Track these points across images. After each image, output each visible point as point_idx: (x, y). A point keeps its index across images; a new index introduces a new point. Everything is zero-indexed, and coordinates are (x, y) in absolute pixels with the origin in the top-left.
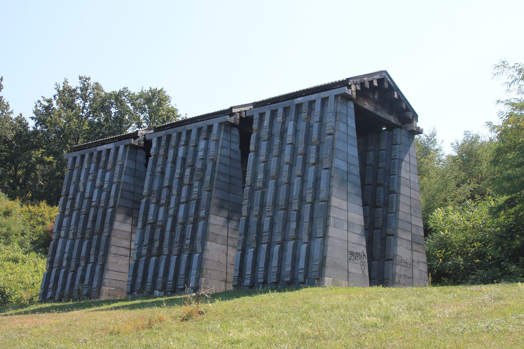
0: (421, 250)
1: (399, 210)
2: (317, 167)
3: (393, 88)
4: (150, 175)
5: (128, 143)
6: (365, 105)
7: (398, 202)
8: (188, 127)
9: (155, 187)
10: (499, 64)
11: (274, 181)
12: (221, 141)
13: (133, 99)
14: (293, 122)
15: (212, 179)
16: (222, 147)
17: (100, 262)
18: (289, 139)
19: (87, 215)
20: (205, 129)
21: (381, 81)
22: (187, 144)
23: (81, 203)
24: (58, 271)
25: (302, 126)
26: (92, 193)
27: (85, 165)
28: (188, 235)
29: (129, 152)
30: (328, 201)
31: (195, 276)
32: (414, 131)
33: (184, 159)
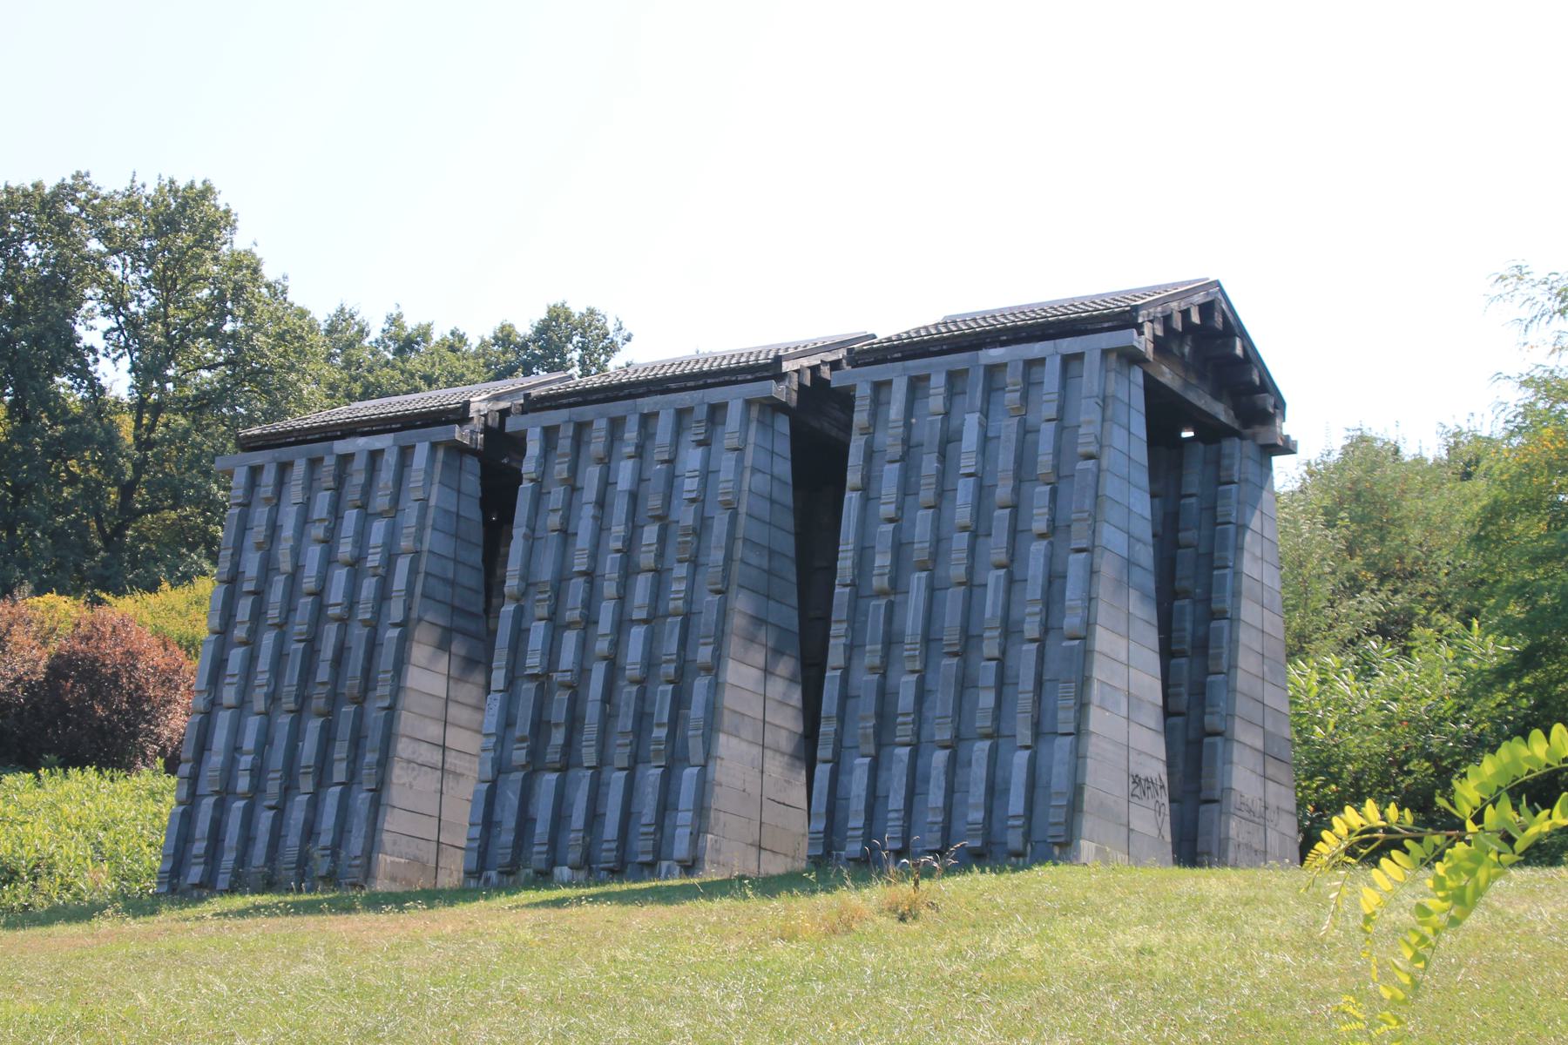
0: (1284, 780)
1: (1236, 667)
2: (1051, 543)
3: (1233, 329)
4: (526, 537)
6: (1162, 374)
7: (1234, 642)
8: (647, 404)
9: (546, 571)
10: (1507, 274)
11: (924, 574)
12: (750, 450)
13: (99, 214)
14: (977, 415)
15: (728, 558)
16: (754, 470)
17: (368, 779)
18: (968, 463)
20: (701, 413)
21: (1207, 309)
22: (640, 453)
23: (289, 608)
24: (221, 807)
25: (1007, 428)
26: (324, 579)
27: (295, 493)
28: (661, 712)
29: (444, 463)
30: (1085, 637)
31: (688, 830)
32: (1276, 446)
33: (634, 497)
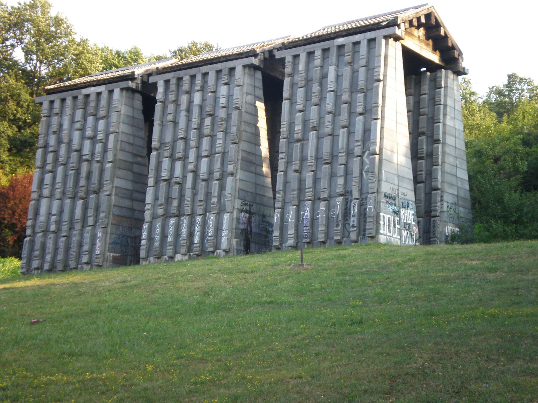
2: (365, 117)
5: (125, 86)
11: (315, 132)
18: (331, 86)
19: (78, 171)
